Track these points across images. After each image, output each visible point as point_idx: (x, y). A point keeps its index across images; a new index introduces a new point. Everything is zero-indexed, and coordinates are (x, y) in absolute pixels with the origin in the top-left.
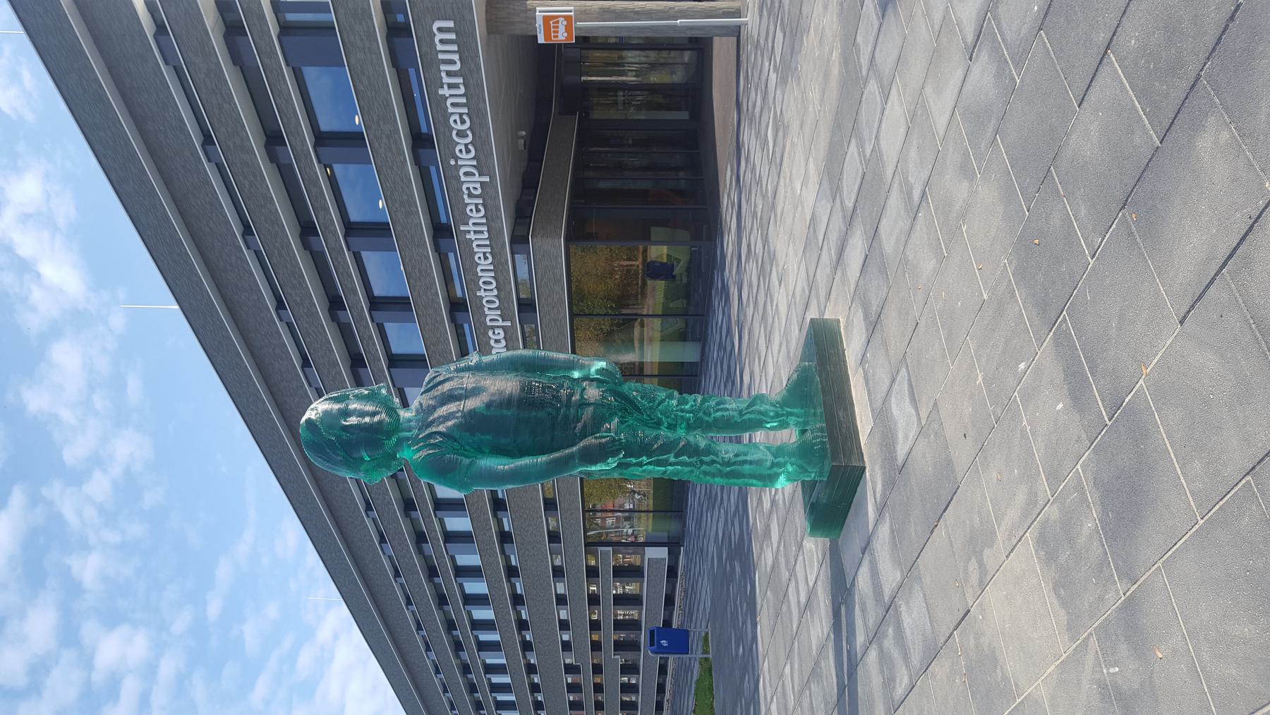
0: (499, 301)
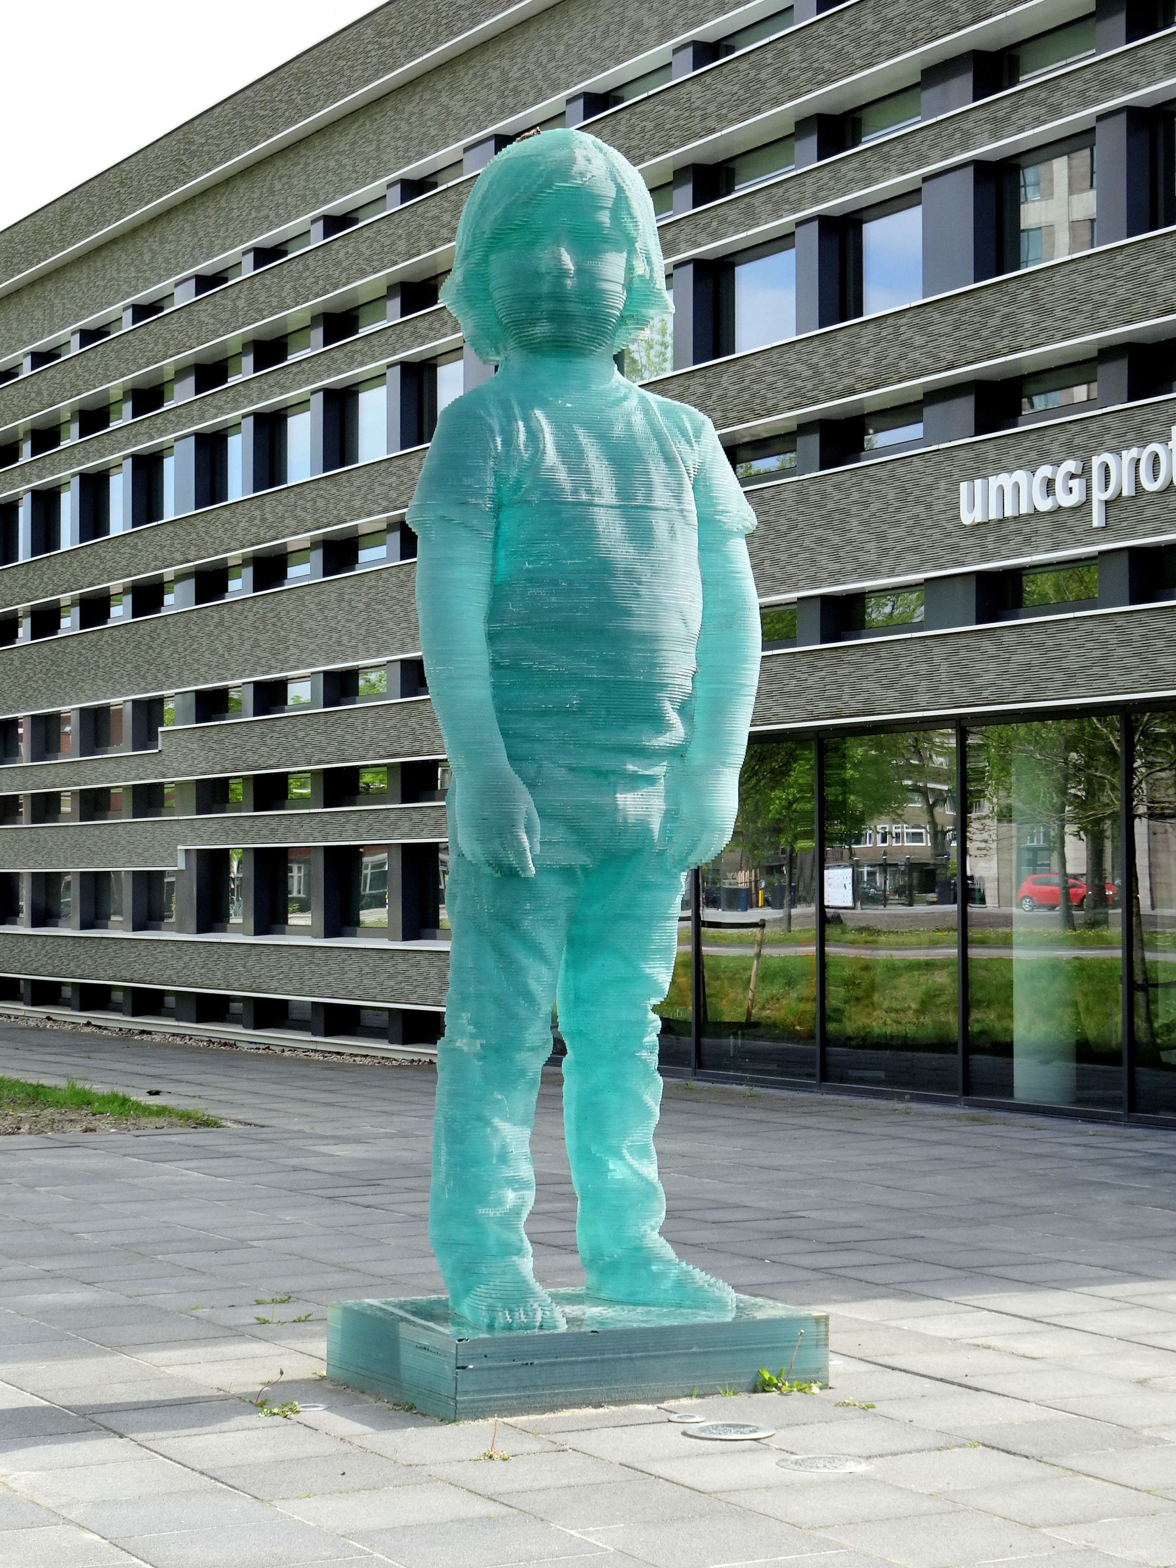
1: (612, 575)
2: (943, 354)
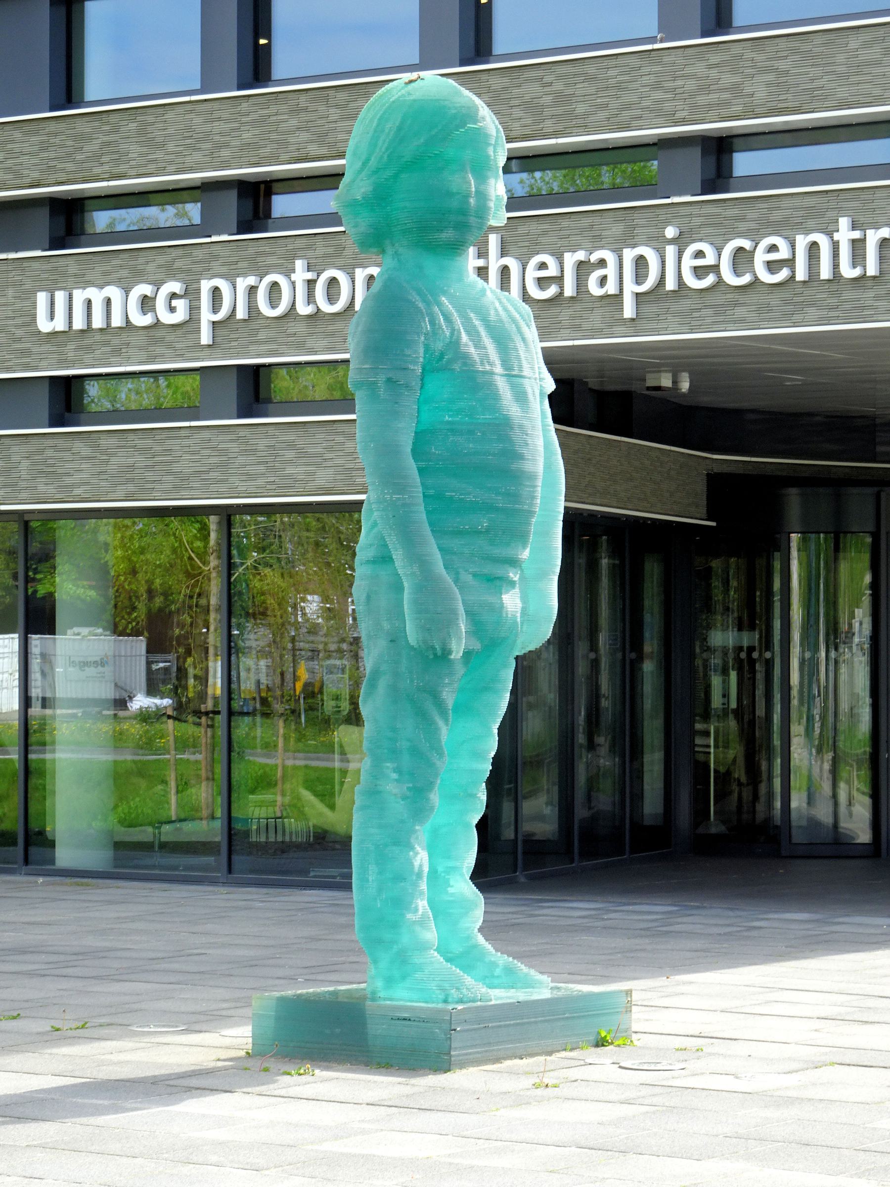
0: (702, 290)
1: (512, 428)
2: (26, 172)
